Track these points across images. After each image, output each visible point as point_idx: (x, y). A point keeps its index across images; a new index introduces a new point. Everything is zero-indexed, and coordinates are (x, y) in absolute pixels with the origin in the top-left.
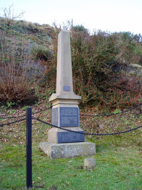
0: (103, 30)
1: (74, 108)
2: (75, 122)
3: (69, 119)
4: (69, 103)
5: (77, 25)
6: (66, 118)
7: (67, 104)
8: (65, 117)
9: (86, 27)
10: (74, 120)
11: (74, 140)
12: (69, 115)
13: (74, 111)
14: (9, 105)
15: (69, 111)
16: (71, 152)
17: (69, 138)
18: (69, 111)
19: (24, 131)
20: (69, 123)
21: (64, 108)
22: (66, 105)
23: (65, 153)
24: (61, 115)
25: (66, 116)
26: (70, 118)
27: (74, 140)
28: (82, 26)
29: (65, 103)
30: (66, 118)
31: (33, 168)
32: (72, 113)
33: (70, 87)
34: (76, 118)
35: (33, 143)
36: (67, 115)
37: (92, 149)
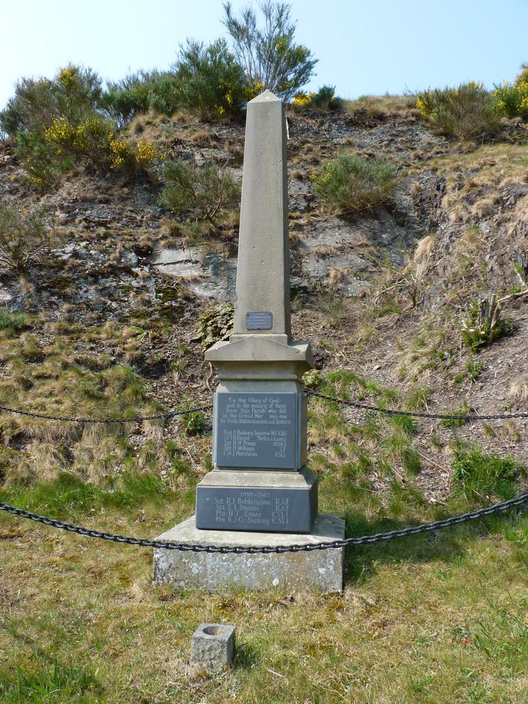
1: (275, 396)
2: (278, 449)
3: (253, 439)
4: (256, 377)
5: (21, 81)
6: (244, 433)
7: (263, 383)
8: (239, 431)
9: (366, 94)
11: (264, 521)
12: (253, 422)
13: (278, 409)
15: (257, 406)
16: (228, 570)
17: (241, 513)
18: (257, 406)
20: (254, 455)
23: (206, 570)
24: (223, 421)
26: (257, 434)
27: (264, 521)
29: (240, 376)
30: (244, 433)
32: (266, 416)
37: (322, 571)
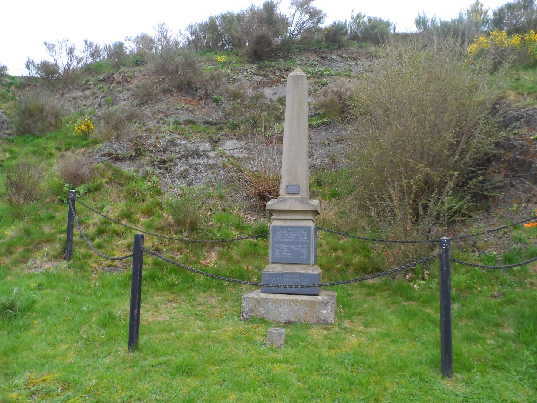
0: (48, 61)
2: (302, 254)
3: (290, 249)
6: (286, 246)
10: (301, 252)
12: (290, 240)
13: (303, 234)
14: (406, 175)
15: (293, 232)
19: (36, 324)
21: (281, 227)
22: (286, 221)
25: (285, 243)
28: (335, 23)
29: (283, 217)
31: (141, 316)
32: (297, 237)
33: (299, 186)
34: (305, 246)
35: (67, 219)
36: (286, 240)
